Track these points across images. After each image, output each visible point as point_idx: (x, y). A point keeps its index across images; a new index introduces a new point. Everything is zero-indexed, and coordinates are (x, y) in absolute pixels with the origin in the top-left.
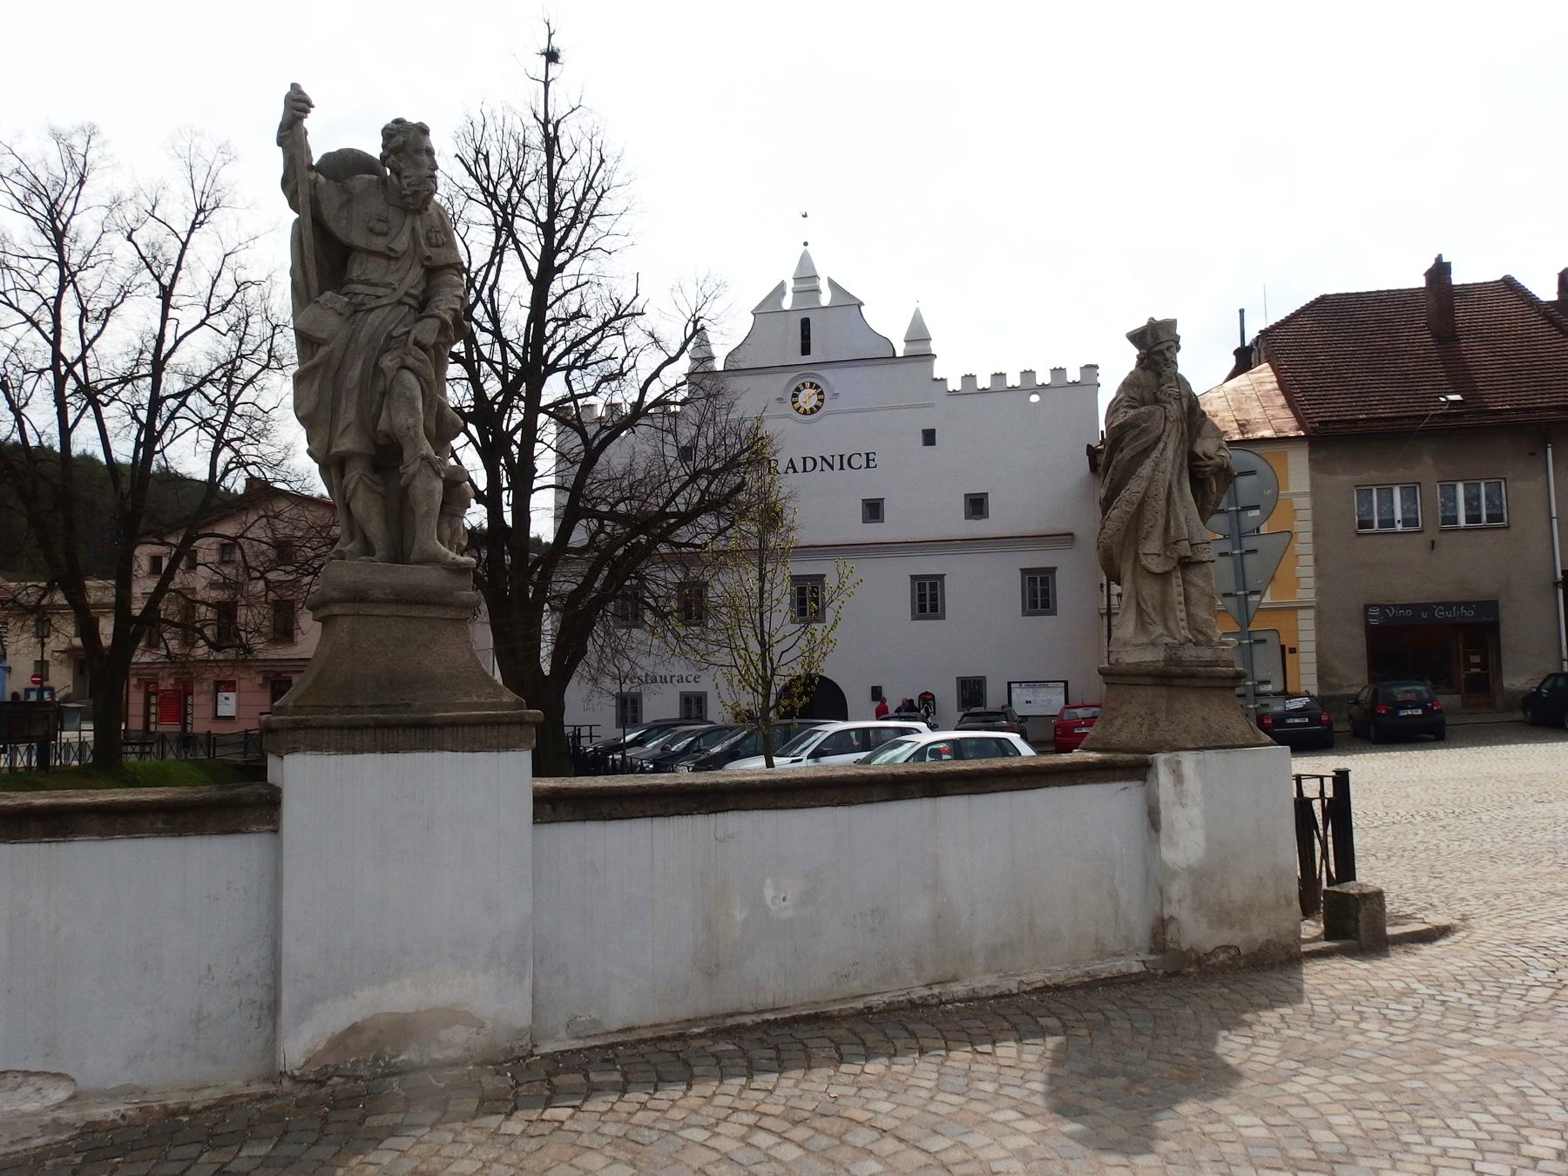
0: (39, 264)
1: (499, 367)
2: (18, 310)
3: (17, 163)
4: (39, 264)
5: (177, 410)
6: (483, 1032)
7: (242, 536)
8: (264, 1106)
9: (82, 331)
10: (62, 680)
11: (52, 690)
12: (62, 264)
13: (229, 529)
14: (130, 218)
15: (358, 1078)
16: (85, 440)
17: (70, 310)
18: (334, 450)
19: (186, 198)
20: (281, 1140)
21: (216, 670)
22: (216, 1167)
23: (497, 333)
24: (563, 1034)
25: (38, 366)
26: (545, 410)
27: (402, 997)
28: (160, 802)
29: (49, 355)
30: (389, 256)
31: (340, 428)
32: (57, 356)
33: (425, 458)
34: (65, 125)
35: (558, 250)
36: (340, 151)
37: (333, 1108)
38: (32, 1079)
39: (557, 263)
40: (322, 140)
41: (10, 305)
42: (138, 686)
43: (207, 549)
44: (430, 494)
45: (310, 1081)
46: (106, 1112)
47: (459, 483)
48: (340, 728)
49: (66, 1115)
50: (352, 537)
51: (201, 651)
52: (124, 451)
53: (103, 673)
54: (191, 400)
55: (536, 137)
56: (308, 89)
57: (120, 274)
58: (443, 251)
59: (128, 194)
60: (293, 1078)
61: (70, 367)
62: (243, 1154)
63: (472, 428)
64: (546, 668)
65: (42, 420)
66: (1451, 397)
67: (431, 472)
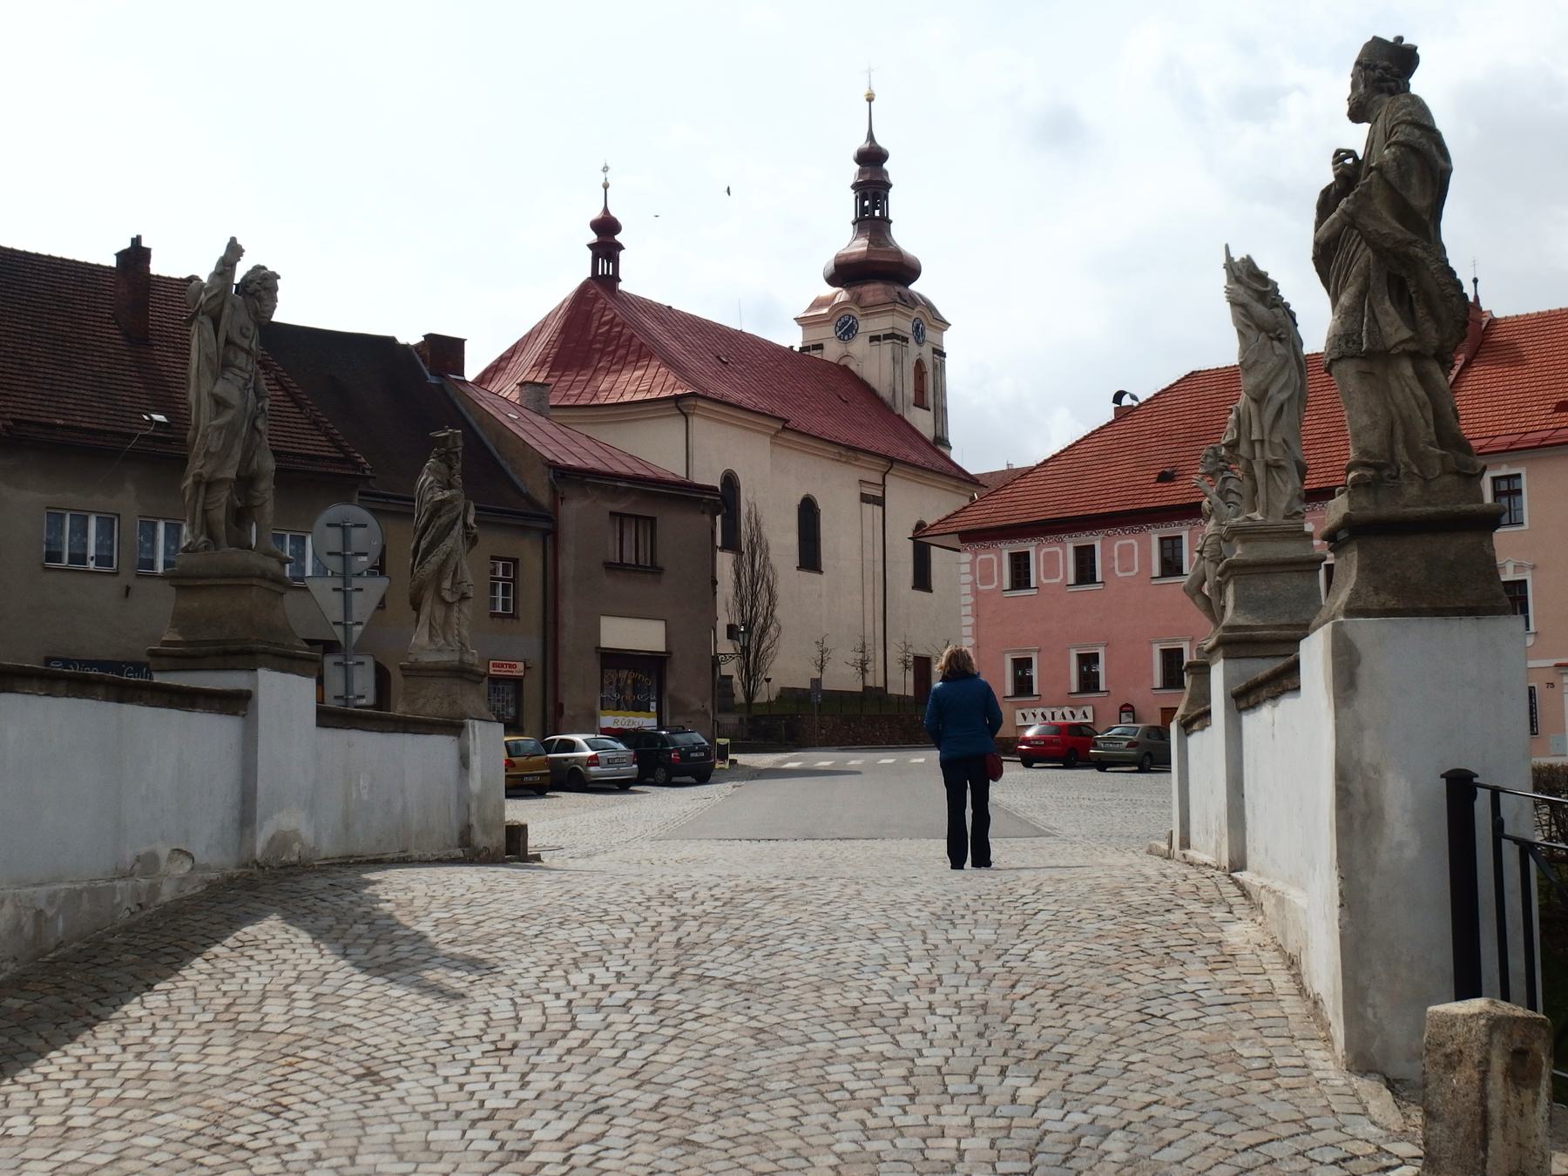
46: (213, 876)
66: (157, 417)
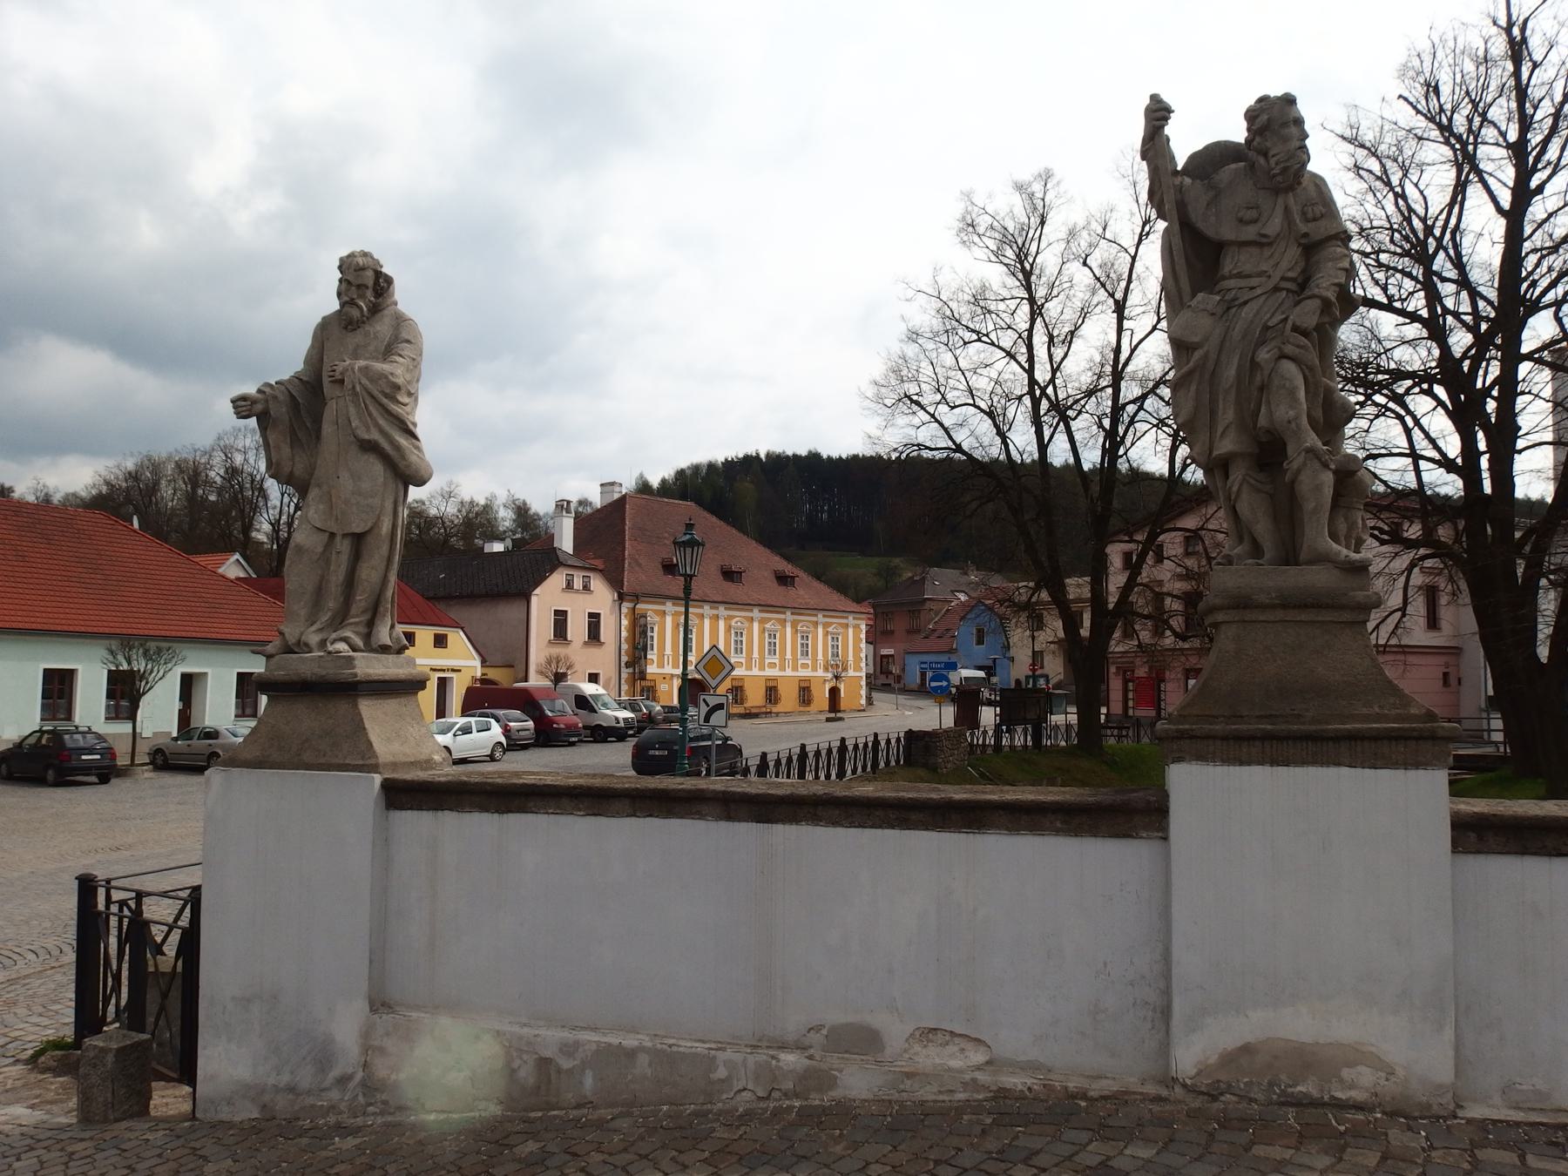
0: (1013, 304)
1: (1468, 318)
2: (999, 347)
3: (990, 220)
4: (1013, 304)
5: (1136, 414)
6: (1393, 1079)
7: (1202, 528)
8: (1156, 1108)
9: (1050, 356)
10: (1055, 667)
11: (1046, 677)
12: (1032, 300)
13: (1190, 522)
14: (1084, 244)
15: (1251, 1100)
16: (1059, 453)
17: (1040, 339)
18: (1215, 453)
19: (1132, 214)
20: (1165, 1147)
21: (1183, 659)
22: (1099, 1159)
23: (1464, 282)
24: (1497, 1100)
25: (1018, 392)
26: (1529, 357)
27: (1298, 1025)
28: (1057, 803)
29: (1026, 382)
30: (1262, 243)
31: (1220, 430)
32: (1032, 382)
33: (1311, 451)
34: (1025, 176)
35: (1535, 170)
36: (1207, 148)
37: (1222, 1126)
38: (957, 1040)
39: (1534, 183)
40: (1184, 142)
41: (993, 344)
42: (1117, 674)
43: (1172, 543)
44: (1318, 488)
45: (1202, 1093)
46: (1015, 1081)
47: (1354, 473)
48: (1225, 738)
49: (982, 1077)
50: (1241, 540)
51: (1169, 641)
52: (1091, 457)
53: (1086, 662)
54: (1148, 403)
55: (1499, 46)
56: (1166, 97)
57: (1080, 296)
58: (1323, 223)
59: (1081, 223)
60: (1184, 1086)
61: (1043, 390)
62: (1127, 1152)
63: (1440, 391)
64: (1543, 653)
65: (1023, 440)
67: (1317, 465)
